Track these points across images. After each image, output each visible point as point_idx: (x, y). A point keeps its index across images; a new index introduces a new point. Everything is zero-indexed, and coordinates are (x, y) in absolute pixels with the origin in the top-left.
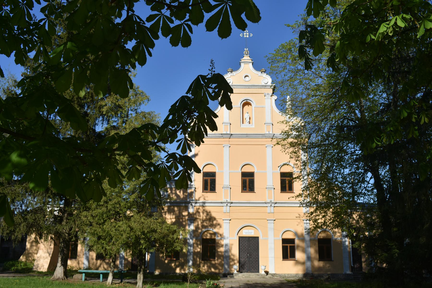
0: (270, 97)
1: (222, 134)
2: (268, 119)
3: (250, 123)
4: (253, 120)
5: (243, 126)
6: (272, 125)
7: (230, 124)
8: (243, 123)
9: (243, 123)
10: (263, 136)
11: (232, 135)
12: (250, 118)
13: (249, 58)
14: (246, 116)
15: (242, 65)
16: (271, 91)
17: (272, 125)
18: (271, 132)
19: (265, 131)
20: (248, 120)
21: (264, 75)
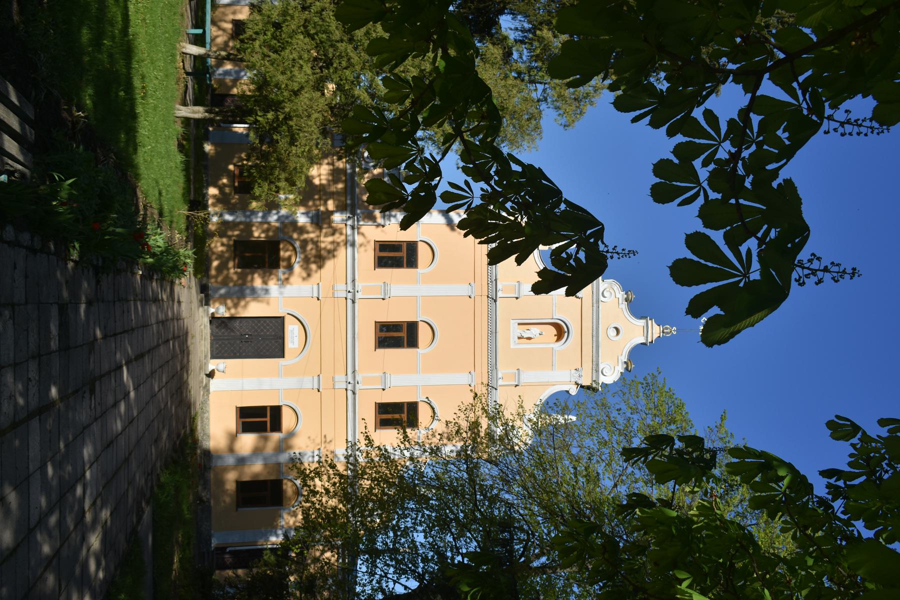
0: (573, 380)
1: (496, 280)
2: (527, 377)
3: (519, 338)
4: (525, 345)
5: (513, 324)
6: (516, 386)
7: (517, 298)
8: (519, 324)
9: (519, 324)
10: (493, 367)
11: (495, 301)
12: (529, 338)
13: (656, 336)
14: (535, 331)
15: (642, 322)
16: (586, 382)
17: (516, 386)
18: (500, 382)
19: (502, 371)
20: (525, 336)
21: (620, 368)
